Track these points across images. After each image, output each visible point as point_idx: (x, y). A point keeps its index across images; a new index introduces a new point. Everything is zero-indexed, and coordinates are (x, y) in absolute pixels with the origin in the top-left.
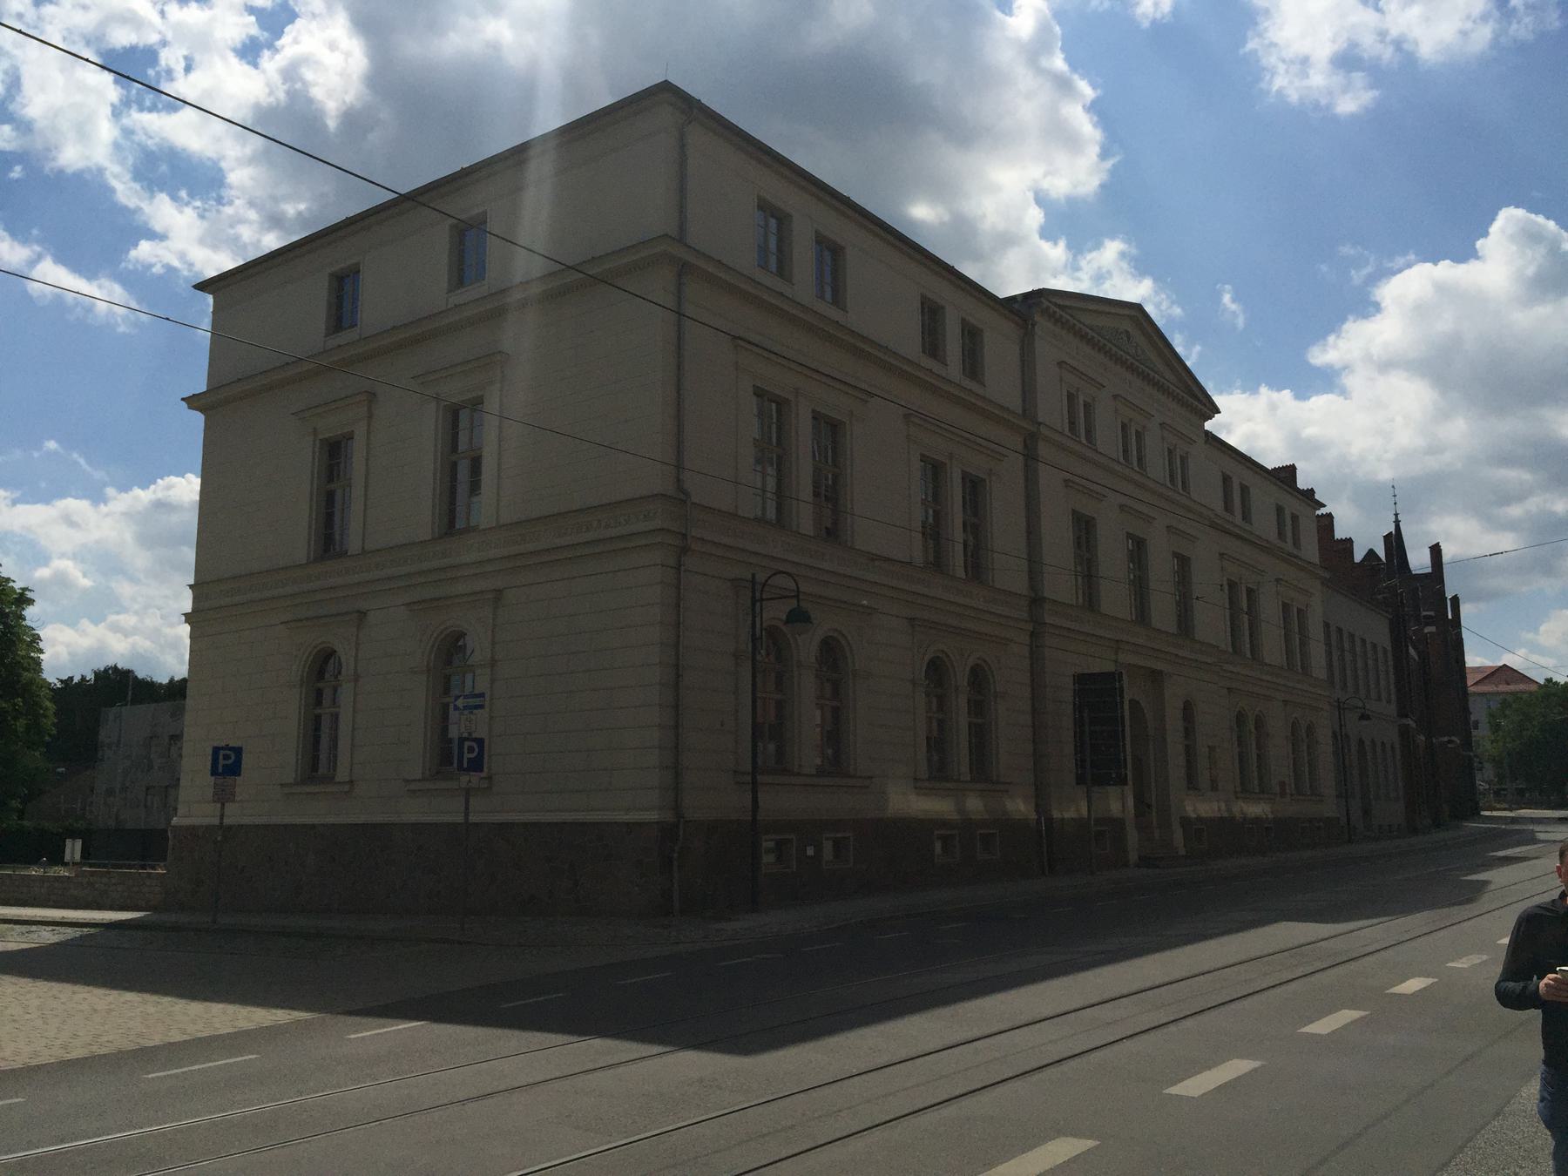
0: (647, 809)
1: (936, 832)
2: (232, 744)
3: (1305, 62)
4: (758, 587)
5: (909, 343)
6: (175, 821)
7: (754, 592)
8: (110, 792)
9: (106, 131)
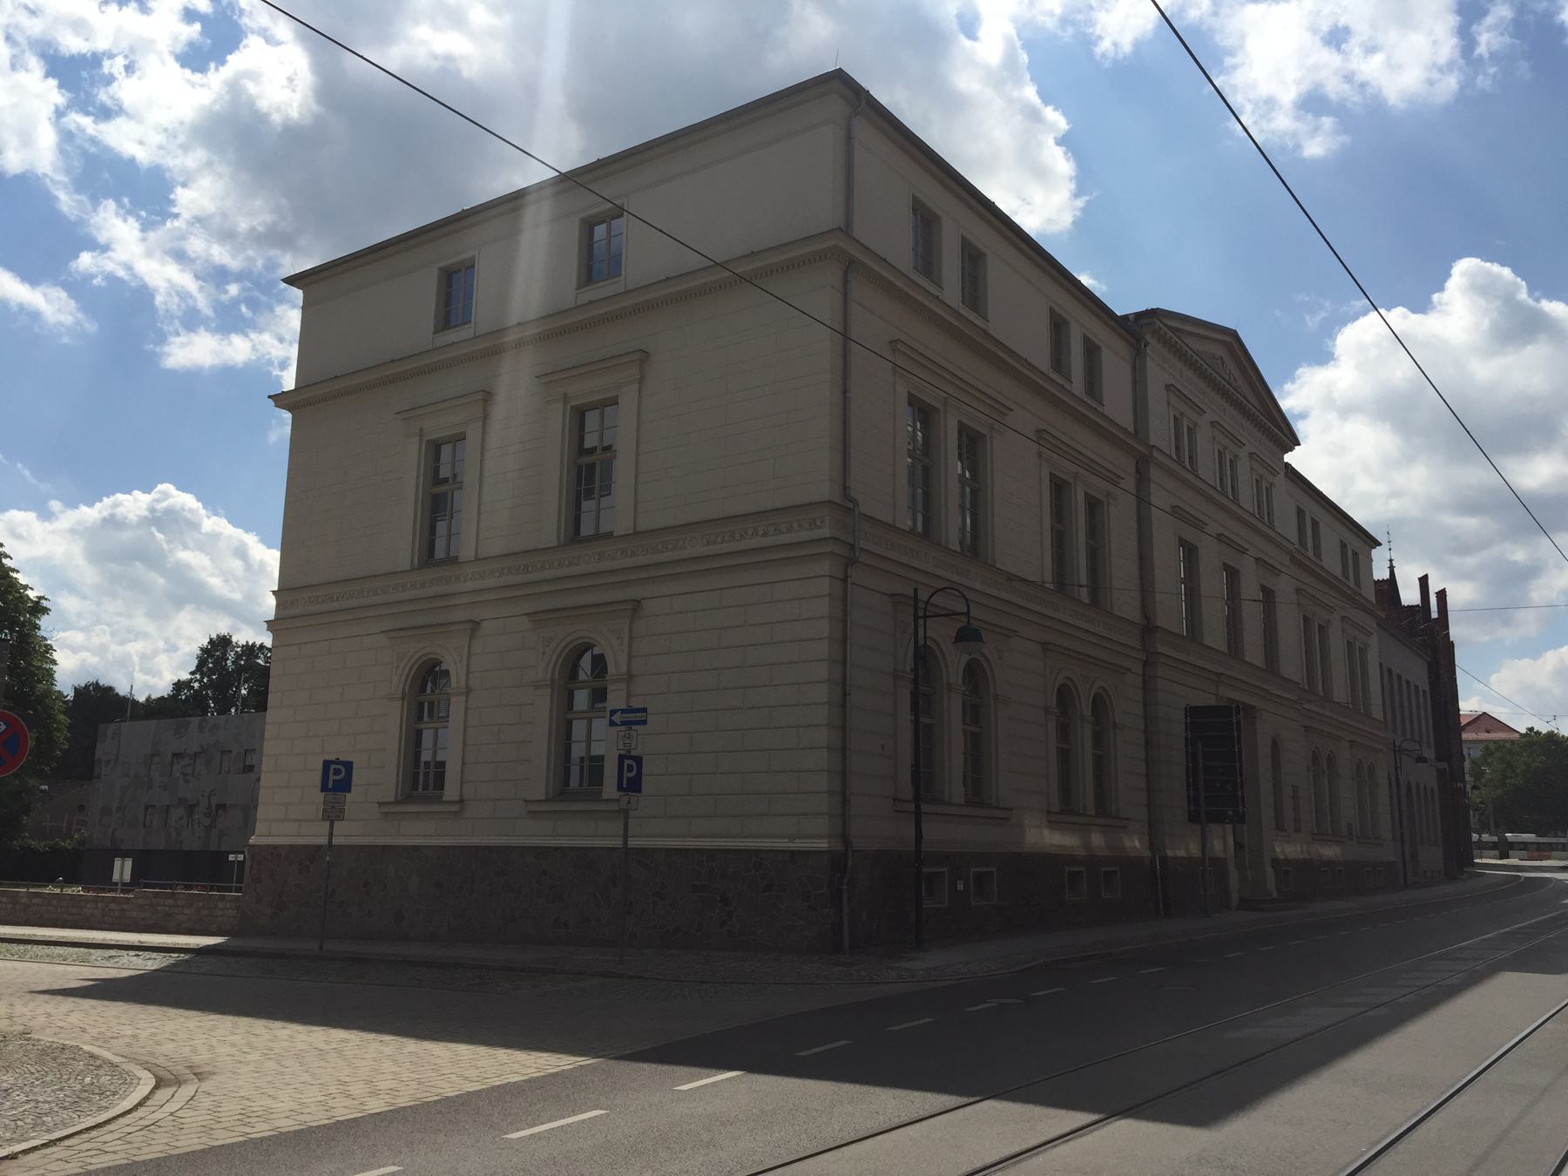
1: (972, 870)
2: (342, 759)
3: (1270, 103)
4: (921, 605)
6: (252, 841)
7: (916, 609)
9: (47, 136)
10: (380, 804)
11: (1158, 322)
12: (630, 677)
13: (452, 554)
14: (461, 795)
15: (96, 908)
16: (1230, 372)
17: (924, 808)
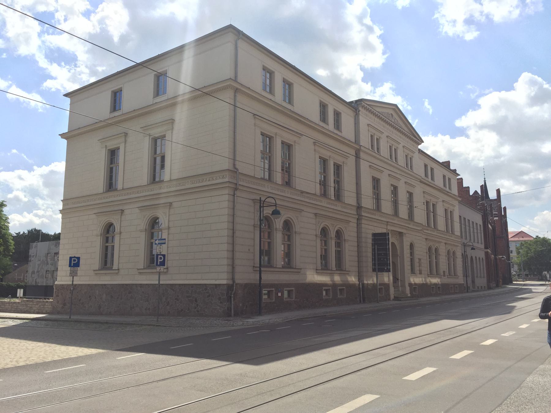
0: (223, 280)
4: (262, 202)
6: (56, 283)
8: (33, 273)
10: (94, 270)
11: (363, 103)
12: (120, 233)
13: (116, 188)
14: (118, 267)
15: (9, 305)
16: (395, 118)
17: (262, 269)
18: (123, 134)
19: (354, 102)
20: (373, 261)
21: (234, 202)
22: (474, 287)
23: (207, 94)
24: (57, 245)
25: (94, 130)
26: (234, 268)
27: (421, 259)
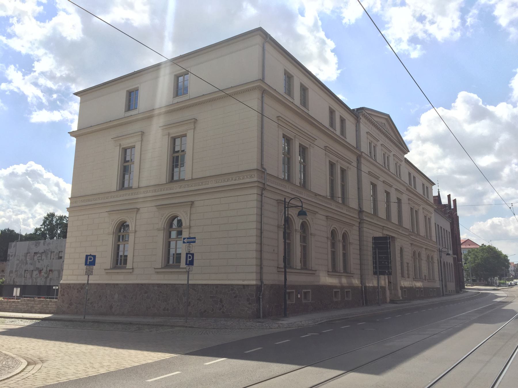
0: (252, 280)
2: (92, 254)
4: (287, 204)
5: (326, 122)
6: (61, 282)
8: (11, 272)
10: (105, 269)
11: (363, 111)
12: (190, 227)
14: (132, 267)
15: (8, 305)
17: (287, 270)
18: (140, 133)
19: (355, 110)
20: (373, 264)
21: (262, 201)
22: (446, 292)
23: (230, 95)
24: (38, 245)
25: (82, 135)
26: (262, 269)
27: (408, 263)
